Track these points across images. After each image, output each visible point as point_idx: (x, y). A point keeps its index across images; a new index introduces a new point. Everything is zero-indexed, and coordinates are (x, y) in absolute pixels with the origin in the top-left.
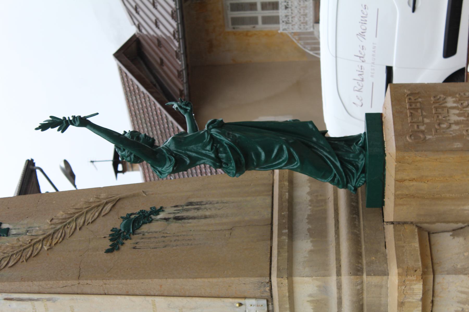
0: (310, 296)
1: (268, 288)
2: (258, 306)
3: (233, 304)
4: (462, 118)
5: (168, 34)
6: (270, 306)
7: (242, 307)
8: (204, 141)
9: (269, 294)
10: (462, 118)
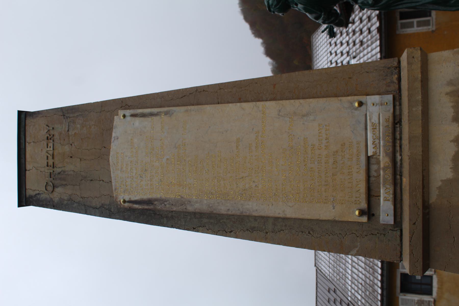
0: (450, 83)
1: (396, 76)
2: (381, 104)
3: (352, 103)
5: (318, 65)
6: (397, 107)
7: (363, 107)
8: (338, 11)
9: (397, 86)
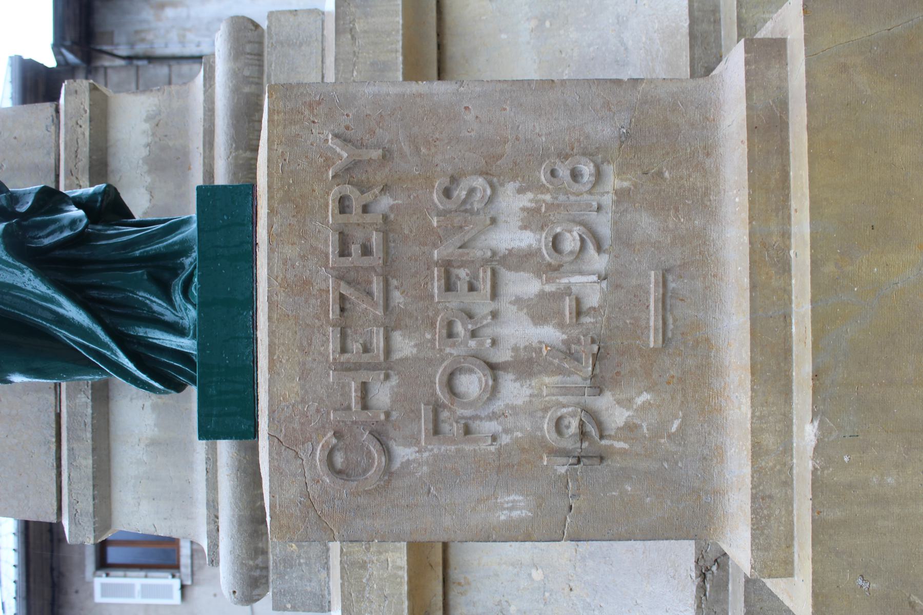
4: (550, 334)
10: (550, 334)
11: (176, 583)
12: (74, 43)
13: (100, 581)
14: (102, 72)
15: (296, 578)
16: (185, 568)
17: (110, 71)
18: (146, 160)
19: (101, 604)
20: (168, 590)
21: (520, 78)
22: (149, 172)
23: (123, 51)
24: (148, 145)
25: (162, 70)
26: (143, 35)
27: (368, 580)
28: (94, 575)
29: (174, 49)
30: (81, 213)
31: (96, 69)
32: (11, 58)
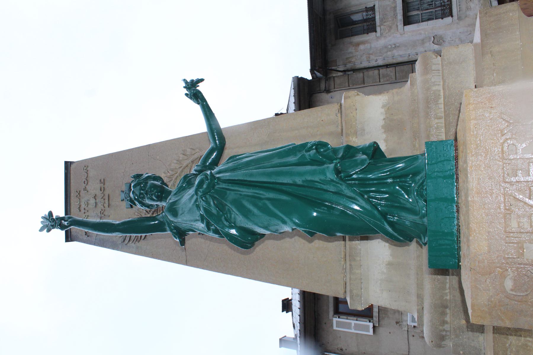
11: (371, 325)
12: (320, 68)
13: (335, 320)
14: (332, 79)
15: (465, 338)
16: (375, 319)
17: (336, 78)
18: (383, 127)
19: (336, 330)
20: (367, 328)
21: (424, 23)
22: (385, 132)
23: (341, 68)
24: (384, 119)
25: (360, 75)
26: (350, 59)
27: (510, 345)
28: (333, 317)
29: (365, 64)
30: (364, 157)
31: (330, 78)
32: (293, 78)
